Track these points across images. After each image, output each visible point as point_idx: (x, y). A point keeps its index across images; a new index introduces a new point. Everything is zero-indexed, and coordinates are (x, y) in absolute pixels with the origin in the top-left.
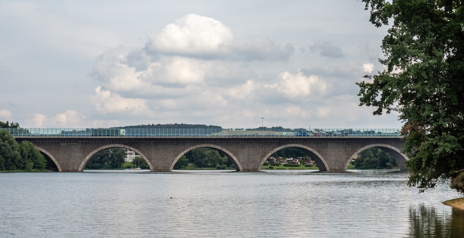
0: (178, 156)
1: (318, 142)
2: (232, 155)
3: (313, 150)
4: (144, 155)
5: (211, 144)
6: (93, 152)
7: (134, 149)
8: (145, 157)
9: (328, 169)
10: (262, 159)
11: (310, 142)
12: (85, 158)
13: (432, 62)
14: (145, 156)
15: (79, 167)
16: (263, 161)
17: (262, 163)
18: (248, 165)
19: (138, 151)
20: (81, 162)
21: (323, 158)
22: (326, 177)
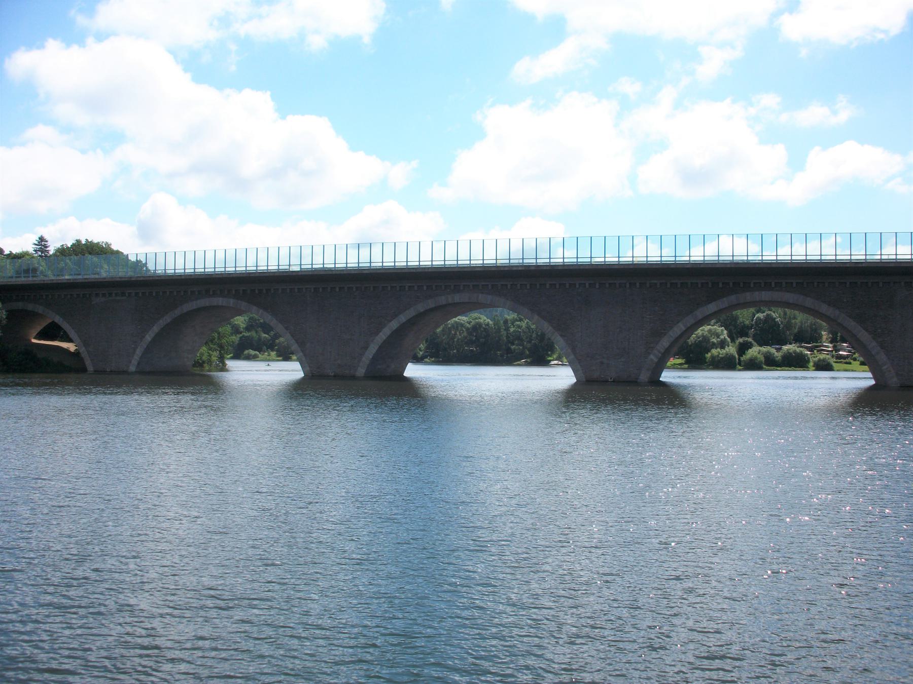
0: (381, 334)
1: (856, 283)
2: (550, 328)
3: (837, 312)
4: (287, 328)
5: (482, 293)
6: (161, 321)
7: (261, 311)
8: (288, 334)
9: (90, 368)
10: (652, 345)
11: (827, 285)
12: (144, 337)
13: (411, 400)
14: (290, 333)
15: (130, 362)
16: (656, 352)
17: (652, 357)
18: (602, 363)
19: (270, 317)
20: (135, 350)
21: (874, 344)
22: (498, 373)
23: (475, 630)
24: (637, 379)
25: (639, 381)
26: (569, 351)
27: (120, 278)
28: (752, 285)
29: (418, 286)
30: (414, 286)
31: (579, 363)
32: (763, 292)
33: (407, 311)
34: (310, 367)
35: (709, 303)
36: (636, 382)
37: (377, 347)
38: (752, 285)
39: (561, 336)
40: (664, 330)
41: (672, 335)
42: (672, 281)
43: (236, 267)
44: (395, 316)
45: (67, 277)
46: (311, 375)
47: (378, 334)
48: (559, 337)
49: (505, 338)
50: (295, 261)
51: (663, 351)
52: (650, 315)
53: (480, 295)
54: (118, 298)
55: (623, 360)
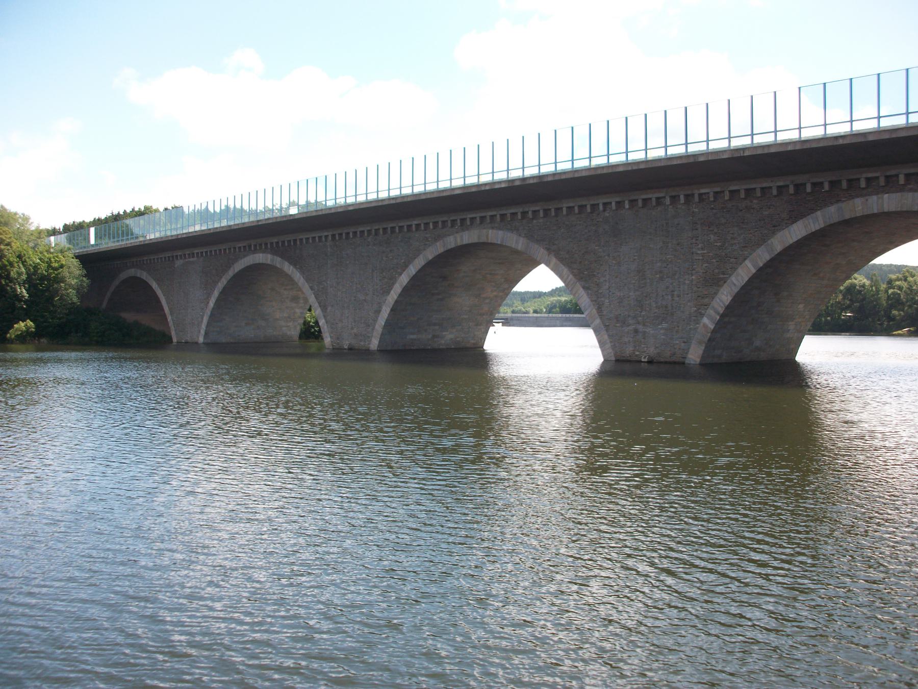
5: (493, 228)
17: (705, 320)
23: (300, 578)
24: (685, 358)
25: (687, 361)
26: (594, 311)
27: (266, 220)
28: (863, 184)
29: (887, 177)
30: (877, 178)
31: (607, 331)
32: (886, 196)
33: (416, 260)
34: (331, 337)
35: (793, 223)
36: (684, 363)
37: (388, 310)
38: (863, 184)
39: (584, 288)
40: (724, 274)
41: (735, 282)
42: (888, 173)
43: (686, 144)
44: (405, 266)
45: (198, 228)
46: (331, 347)
47: (389, 293)
48: (582, 289)
49: (884, 302)
50: (741, 126)
51: (721, 311)
52: (702, 249)
53: (490, 231)
54: (192, 259)
55: (665, 325)
